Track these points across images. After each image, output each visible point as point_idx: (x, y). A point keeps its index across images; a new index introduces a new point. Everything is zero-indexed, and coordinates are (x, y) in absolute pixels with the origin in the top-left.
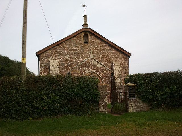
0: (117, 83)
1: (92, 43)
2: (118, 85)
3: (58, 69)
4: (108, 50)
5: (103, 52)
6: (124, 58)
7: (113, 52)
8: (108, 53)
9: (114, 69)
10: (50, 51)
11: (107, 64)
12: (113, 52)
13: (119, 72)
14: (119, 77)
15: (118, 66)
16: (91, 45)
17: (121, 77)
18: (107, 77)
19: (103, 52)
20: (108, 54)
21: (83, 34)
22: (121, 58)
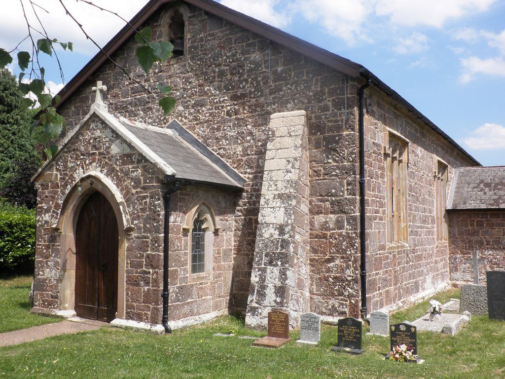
0: (268, 225)
1: (196, 48)
2: (266, 235)
3: (50, 131)
4: (258, 65)
5: (236, 79)
6: (331, 94)
7: (279, 69)
8: (255, 79)
9: (269, 154)
10: (73, 109)
11: (251, 134)
12: (279, 69)
13: (288, 171)
14: (280, 196)
15: (288, 141)
16: (192, 59)
17: (289, 197)
18: (145, 197)
19: (236, 79)
20: (258, 82)
21: (128, 151)
22: (318, 96)
